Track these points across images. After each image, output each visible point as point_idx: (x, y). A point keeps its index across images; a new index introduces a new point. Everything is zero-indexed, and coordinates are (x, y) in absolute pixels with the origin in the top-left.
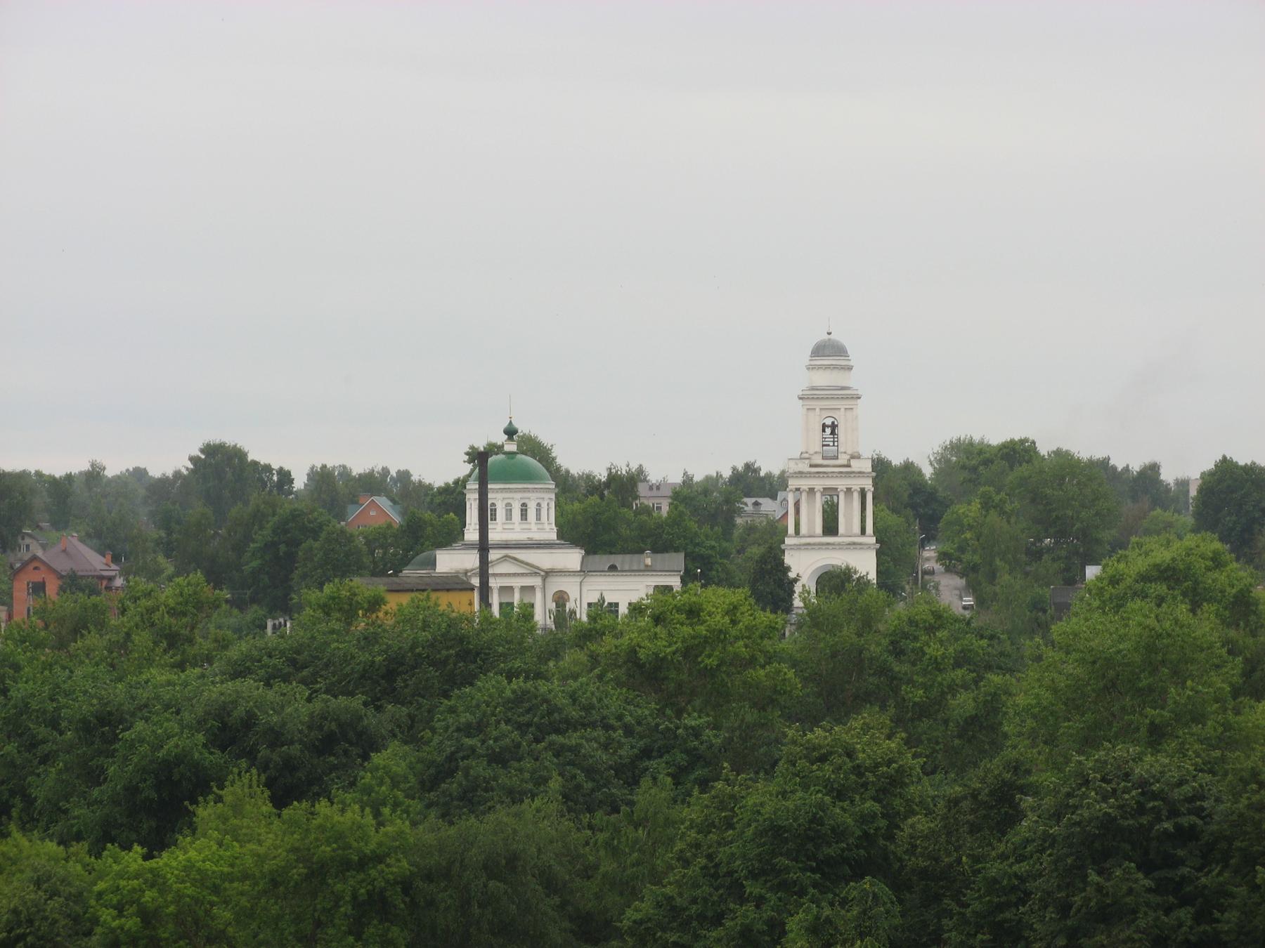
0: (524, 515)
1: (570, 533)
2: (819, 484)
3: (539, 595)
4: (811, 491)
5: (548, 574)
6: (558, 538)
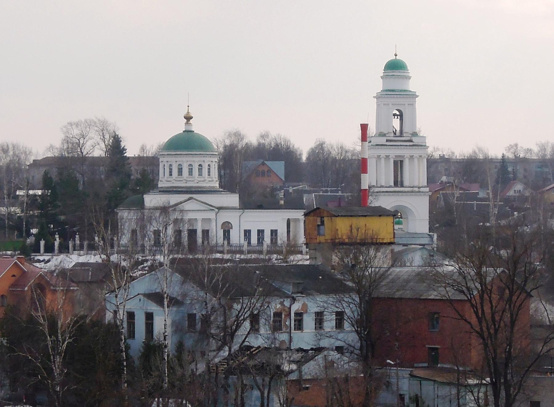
0: (191, 172)
1: (228, 184)
2: (393, 153)
3: (214, 224)
4: (387, 157)
6: (221, 186)
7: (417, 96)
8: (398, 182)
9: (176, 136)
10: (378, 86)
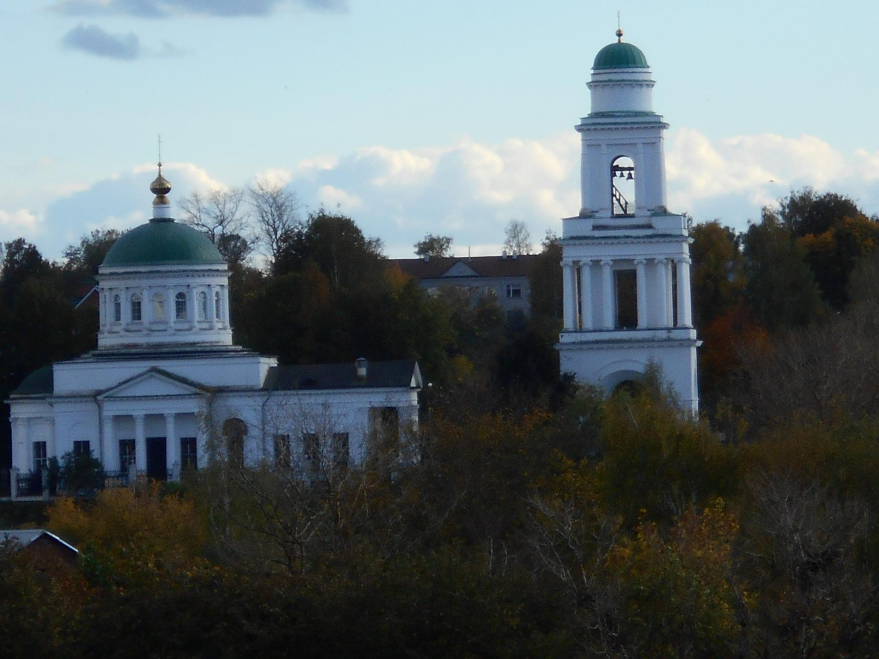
2: (608, 253)
4: (596, 264)
6: (236, 341)
7: (664, 126)
8: (627, 316)
9: (142, 226)
10: (583, 104)
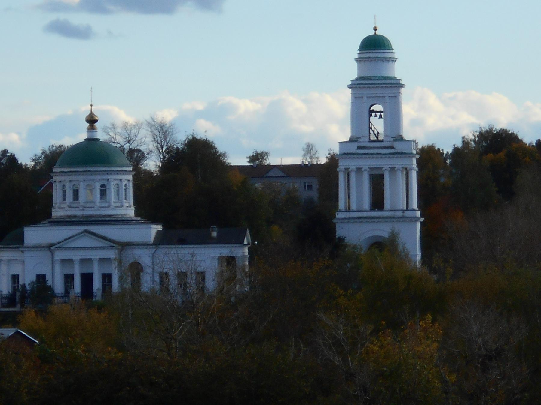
2: (366, 164)
3: (115, 265)
4: (359, 170)
5: (123, 246)
6: (137, 215)
7: (402, 86)
8: (378, 203)
10: (353, 72)
